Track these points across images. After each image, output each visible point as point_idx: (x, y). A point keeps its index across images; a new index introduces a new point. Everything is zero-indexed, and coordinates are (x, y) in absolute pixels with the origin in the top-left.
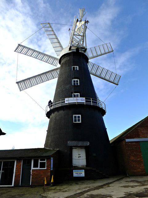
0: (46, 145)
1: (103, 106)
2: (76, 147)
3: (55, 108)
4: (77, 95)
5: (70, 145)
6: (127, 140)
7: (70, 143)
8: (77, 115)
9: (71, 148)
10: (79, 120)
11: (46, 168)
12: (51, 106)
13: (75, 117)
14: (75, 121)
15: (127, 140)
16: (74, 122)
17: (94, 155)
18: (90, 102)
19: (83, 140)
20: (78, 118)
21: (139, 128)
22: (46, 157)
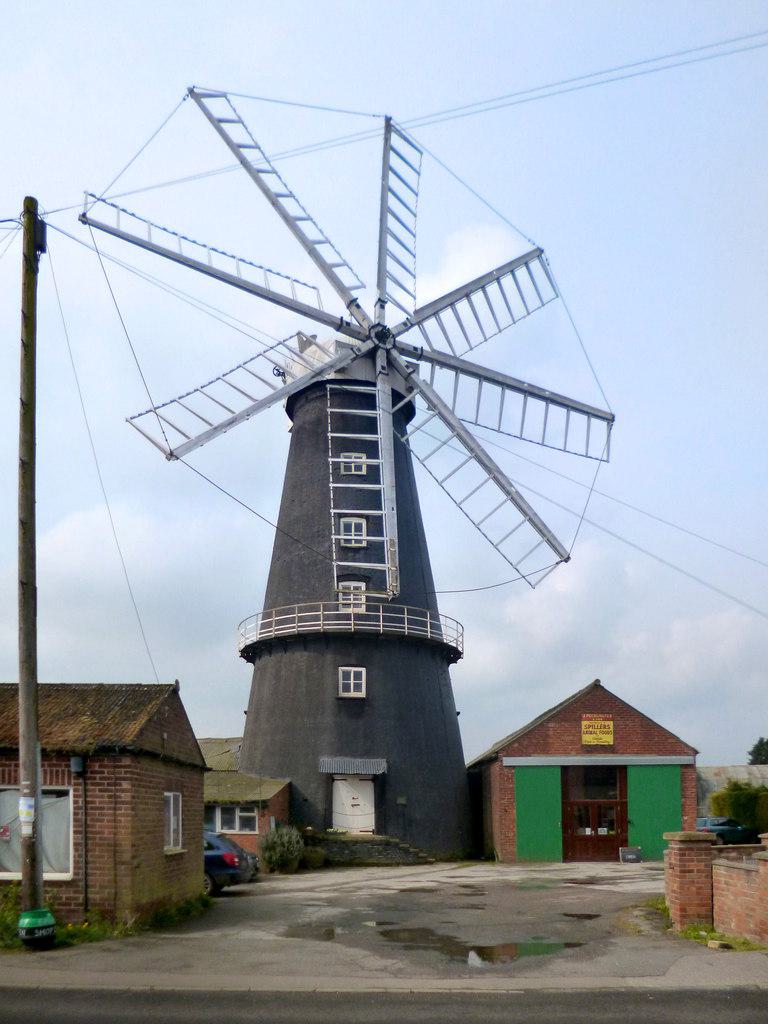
0: (446, 672)
1: (449, 636)
2: (345, 777)
3: (318, 382)
4: (356, 588)
5: (325, 769)
6: (508, 761)
7: (328, 763)
8: (353, 669)
9: (330, 779)
10: (358, 687)
11: (257, 832)
12: (269, 625)
13: (346, 675)
14: (347, 688)
15: (508, 761)
16: (363, 670)
17: (402, 801)
18: (401, 621)
19: (368, 753)
20: (355, 681)
21: (551, 725)
22: (255, 803)
